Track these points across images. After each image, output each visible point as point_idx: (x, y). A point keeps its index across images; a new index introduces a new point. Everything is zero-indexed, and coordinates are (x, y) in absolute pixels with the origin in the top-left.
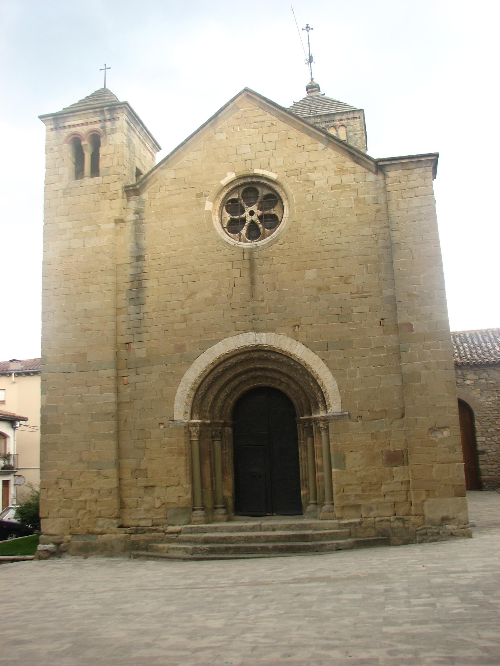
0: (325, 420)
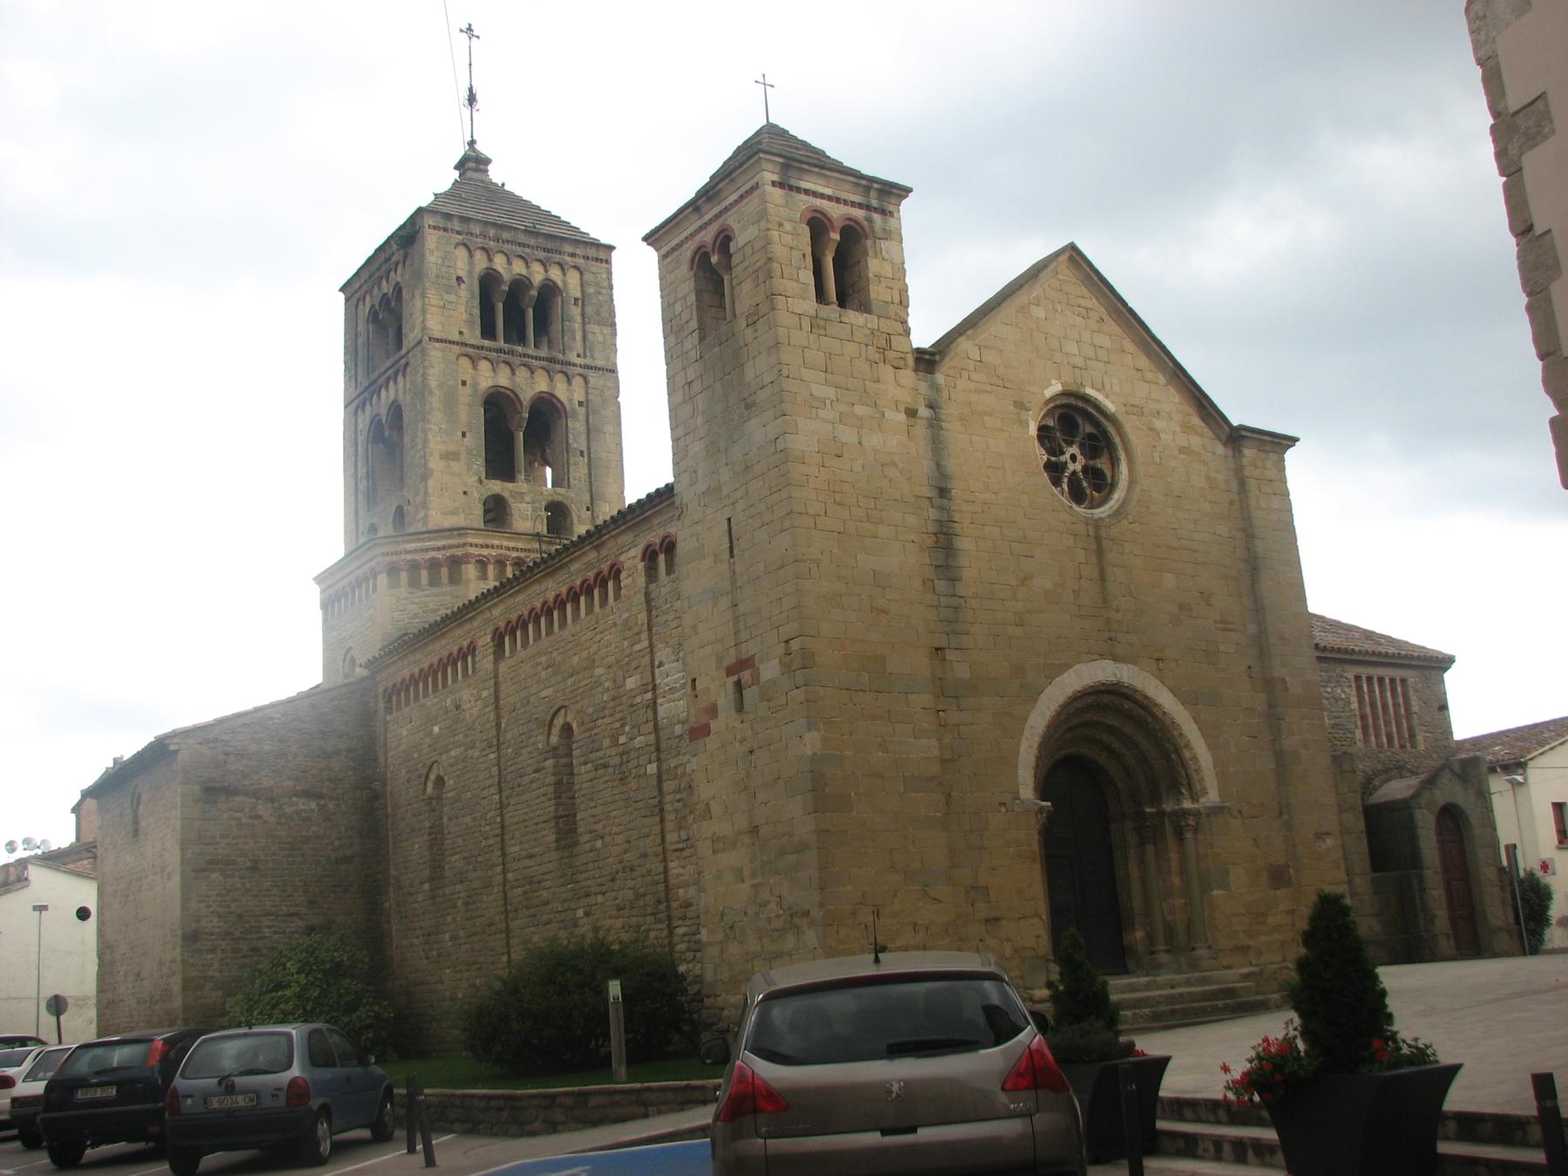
0: (1197, 814)
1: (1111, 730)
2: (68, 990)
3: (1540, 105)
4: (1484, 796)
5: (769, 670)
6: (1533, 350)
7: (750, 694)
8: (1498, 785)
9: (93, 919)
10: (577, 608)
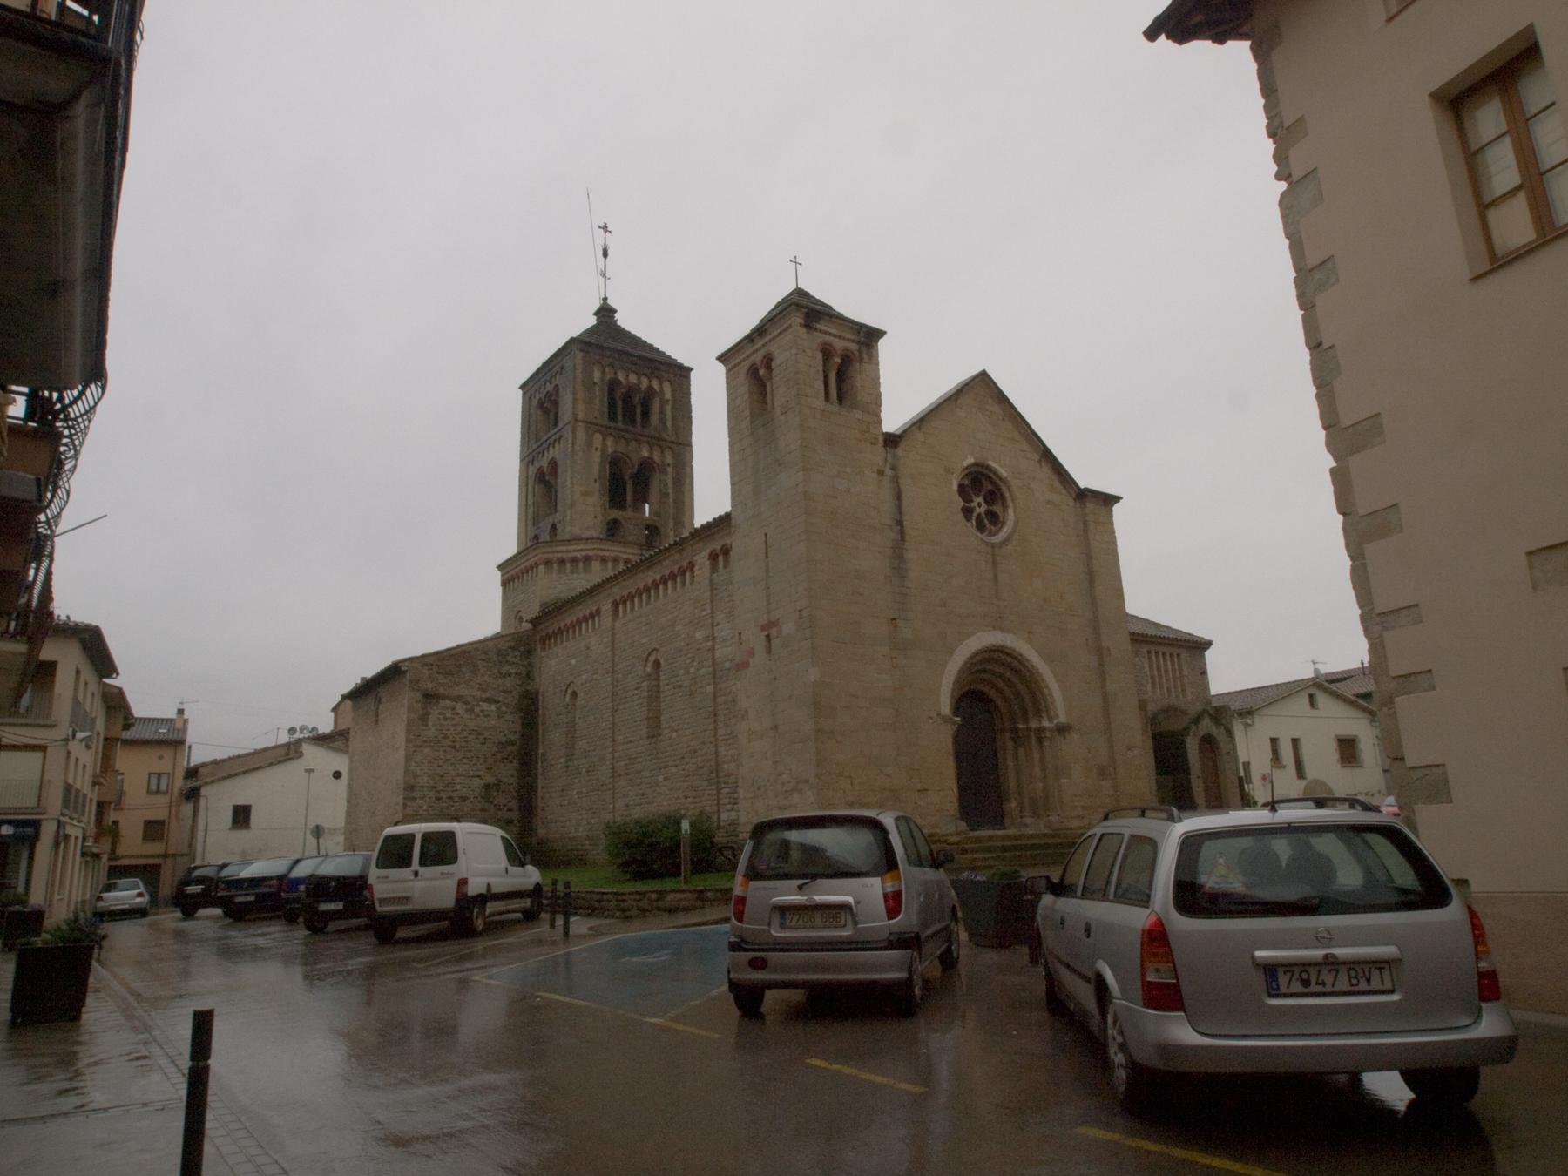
1: (1001, 676)
2: (326, 823)
3: (1329, 264)
4: (1230, 733)
5: (788, 628)
6: (1319, 424)
7: (775, 643)
8: (1238, 728)
9: (345, 777)
10: (666, 589)
